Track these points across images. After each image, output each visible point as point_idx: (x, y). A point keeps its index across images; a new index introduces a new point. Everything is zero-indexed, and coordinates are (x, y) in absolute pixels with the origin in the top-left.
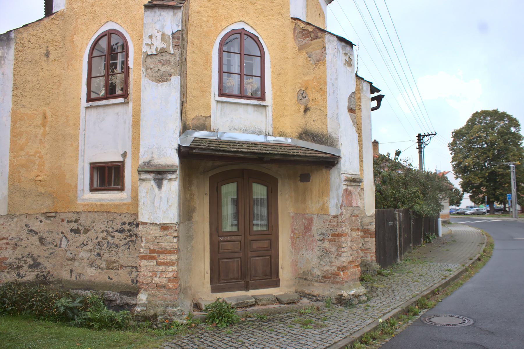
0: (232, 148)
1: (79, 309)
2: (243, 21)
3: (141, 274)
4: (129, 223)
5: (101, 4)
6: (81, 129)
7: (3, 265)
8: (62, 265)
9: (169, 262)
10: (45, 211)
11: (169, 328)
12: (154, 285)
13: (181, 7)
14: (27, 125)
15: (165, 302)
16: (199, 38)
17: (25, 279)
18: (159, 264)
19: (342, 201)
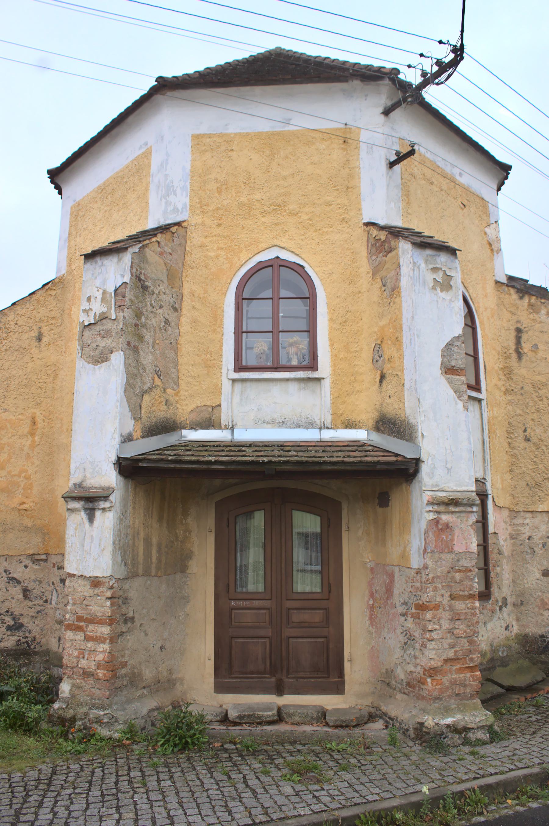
2: (276, 246)
9: (100, 637)
10: (31, 552)
12: (80, 670)
14: (10, 436)
15: (92, 699)
16: (203, 285)
18: (87, 638)
19: (426, 543)
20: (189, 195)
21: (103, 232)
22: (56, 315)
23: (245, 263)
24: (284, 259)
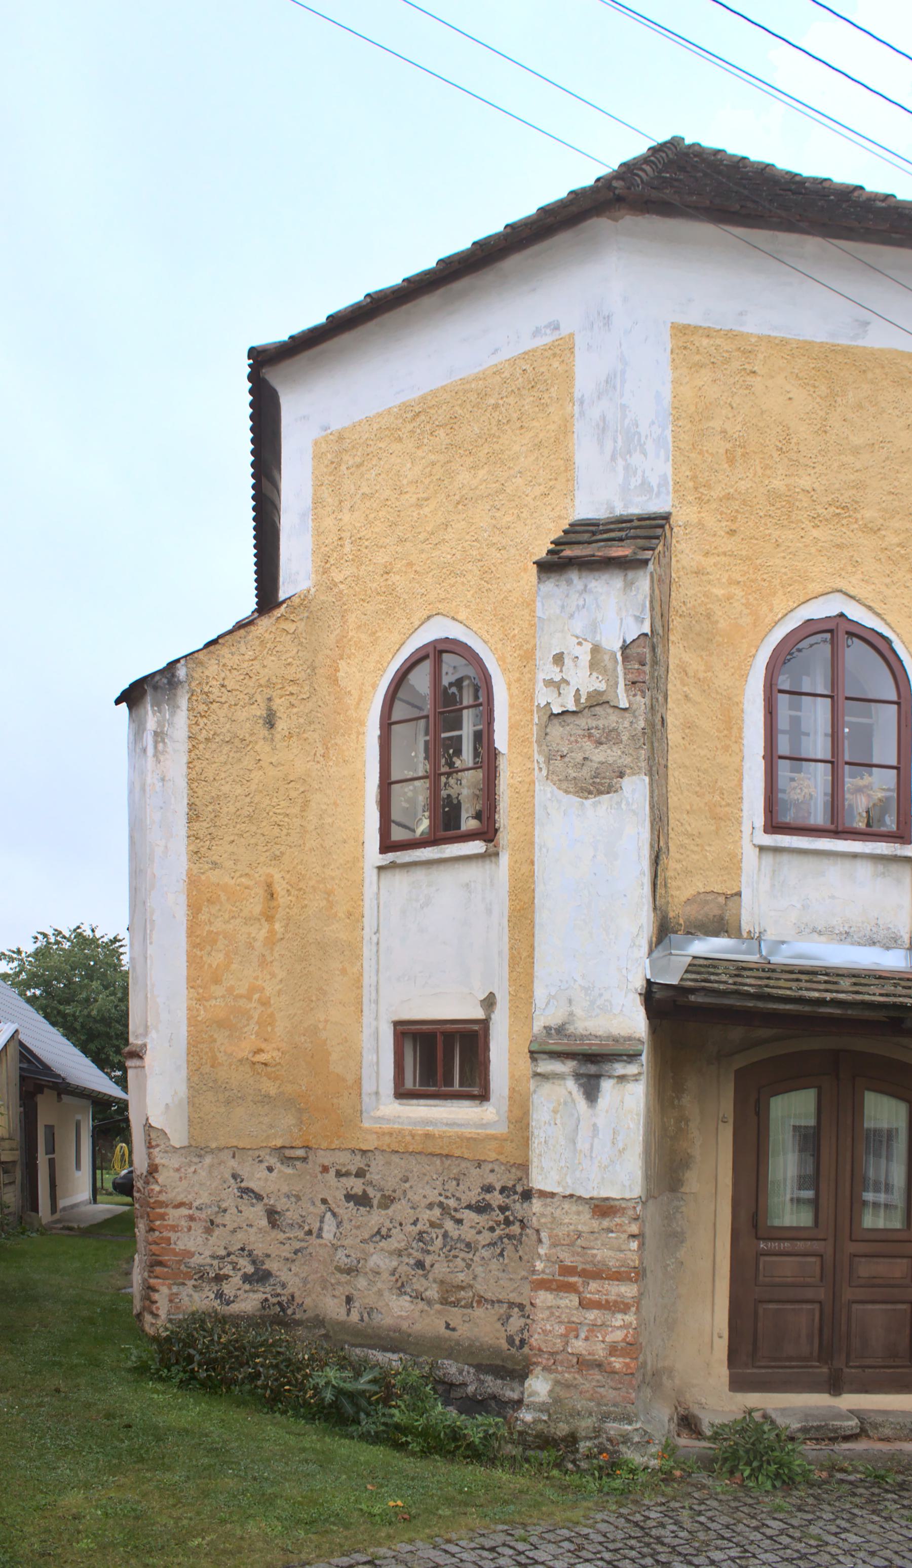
0: (807, 989)
1: (370, 1397)
2: (841, 591)
3: (537, 1328)
4: (503, 1190)
5: (410, 564)
6: (367, 929)
7: (182, 1267)
8: (324, 1283)
9: (616, 1302)
10: (279, 1143)
11: (608, 1475)
12: (570, 1357)
13: (646, 562)
14: (227, 917)
15: (599, 1404)
16: (704, 654)
17: (235, 1308)
18: (585, 1304)
20: (671, 458)
21: (426, 510)
22: (298, 676)
23: (782, 618)
24: (855, 619)
